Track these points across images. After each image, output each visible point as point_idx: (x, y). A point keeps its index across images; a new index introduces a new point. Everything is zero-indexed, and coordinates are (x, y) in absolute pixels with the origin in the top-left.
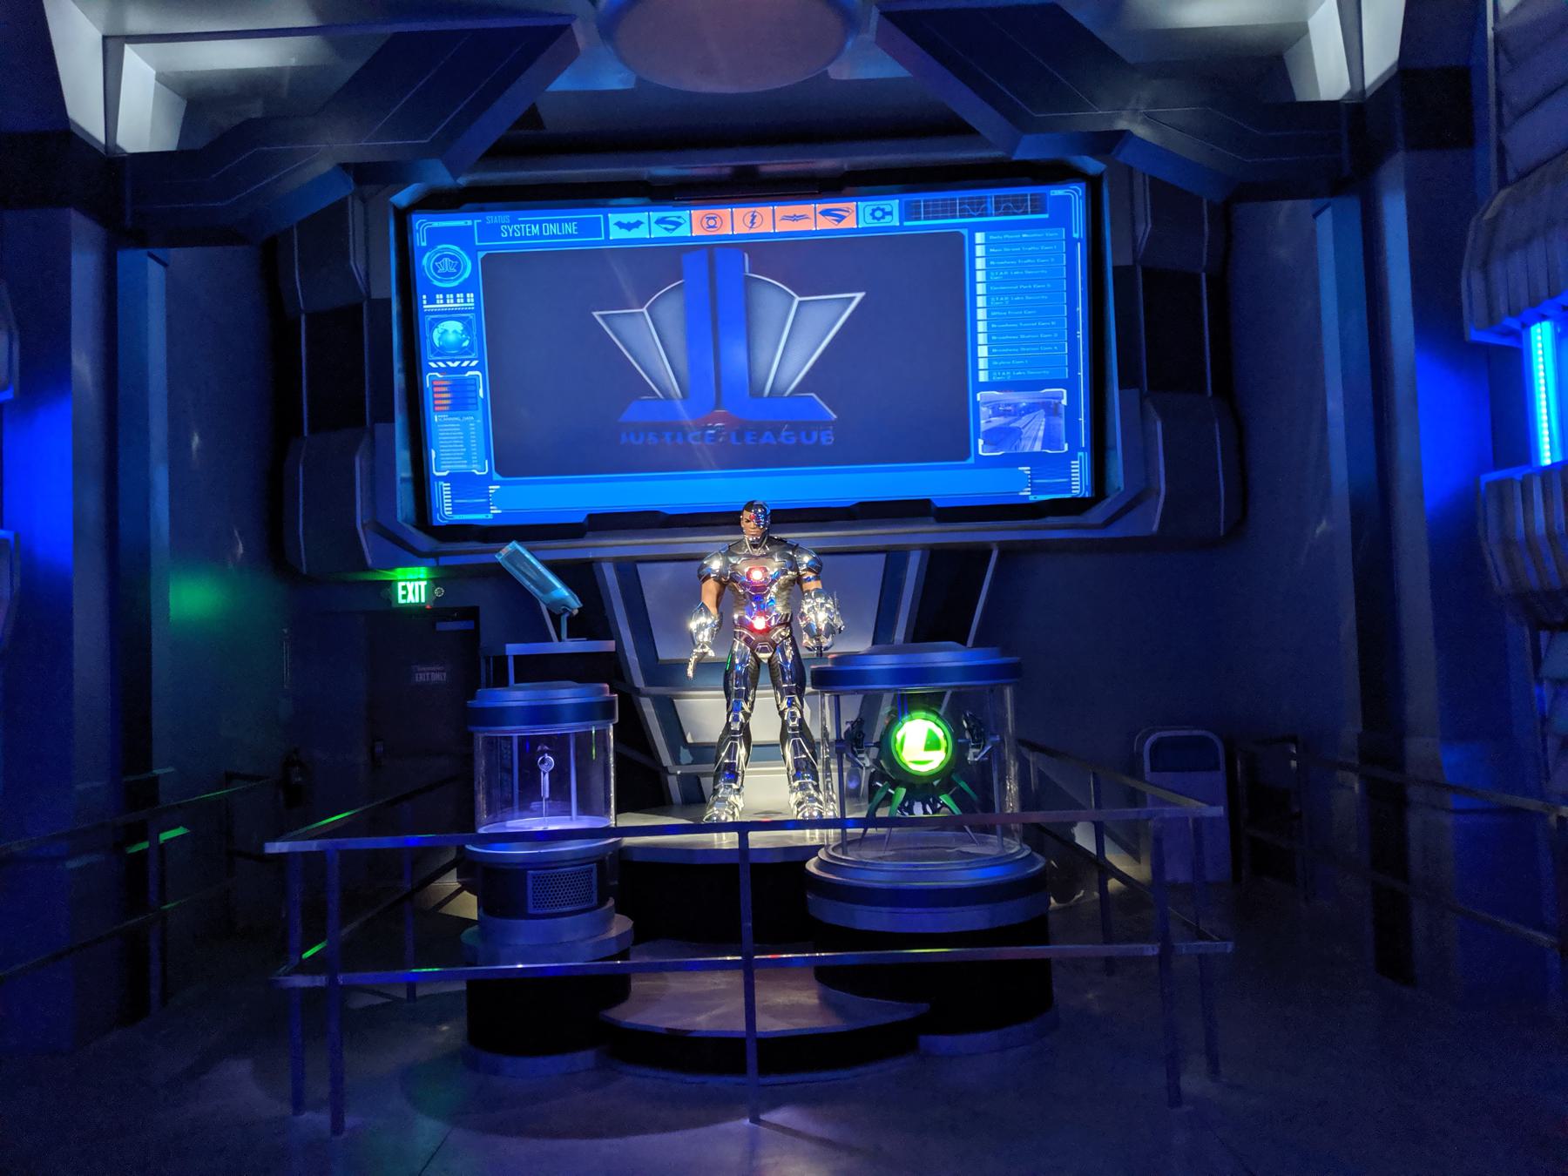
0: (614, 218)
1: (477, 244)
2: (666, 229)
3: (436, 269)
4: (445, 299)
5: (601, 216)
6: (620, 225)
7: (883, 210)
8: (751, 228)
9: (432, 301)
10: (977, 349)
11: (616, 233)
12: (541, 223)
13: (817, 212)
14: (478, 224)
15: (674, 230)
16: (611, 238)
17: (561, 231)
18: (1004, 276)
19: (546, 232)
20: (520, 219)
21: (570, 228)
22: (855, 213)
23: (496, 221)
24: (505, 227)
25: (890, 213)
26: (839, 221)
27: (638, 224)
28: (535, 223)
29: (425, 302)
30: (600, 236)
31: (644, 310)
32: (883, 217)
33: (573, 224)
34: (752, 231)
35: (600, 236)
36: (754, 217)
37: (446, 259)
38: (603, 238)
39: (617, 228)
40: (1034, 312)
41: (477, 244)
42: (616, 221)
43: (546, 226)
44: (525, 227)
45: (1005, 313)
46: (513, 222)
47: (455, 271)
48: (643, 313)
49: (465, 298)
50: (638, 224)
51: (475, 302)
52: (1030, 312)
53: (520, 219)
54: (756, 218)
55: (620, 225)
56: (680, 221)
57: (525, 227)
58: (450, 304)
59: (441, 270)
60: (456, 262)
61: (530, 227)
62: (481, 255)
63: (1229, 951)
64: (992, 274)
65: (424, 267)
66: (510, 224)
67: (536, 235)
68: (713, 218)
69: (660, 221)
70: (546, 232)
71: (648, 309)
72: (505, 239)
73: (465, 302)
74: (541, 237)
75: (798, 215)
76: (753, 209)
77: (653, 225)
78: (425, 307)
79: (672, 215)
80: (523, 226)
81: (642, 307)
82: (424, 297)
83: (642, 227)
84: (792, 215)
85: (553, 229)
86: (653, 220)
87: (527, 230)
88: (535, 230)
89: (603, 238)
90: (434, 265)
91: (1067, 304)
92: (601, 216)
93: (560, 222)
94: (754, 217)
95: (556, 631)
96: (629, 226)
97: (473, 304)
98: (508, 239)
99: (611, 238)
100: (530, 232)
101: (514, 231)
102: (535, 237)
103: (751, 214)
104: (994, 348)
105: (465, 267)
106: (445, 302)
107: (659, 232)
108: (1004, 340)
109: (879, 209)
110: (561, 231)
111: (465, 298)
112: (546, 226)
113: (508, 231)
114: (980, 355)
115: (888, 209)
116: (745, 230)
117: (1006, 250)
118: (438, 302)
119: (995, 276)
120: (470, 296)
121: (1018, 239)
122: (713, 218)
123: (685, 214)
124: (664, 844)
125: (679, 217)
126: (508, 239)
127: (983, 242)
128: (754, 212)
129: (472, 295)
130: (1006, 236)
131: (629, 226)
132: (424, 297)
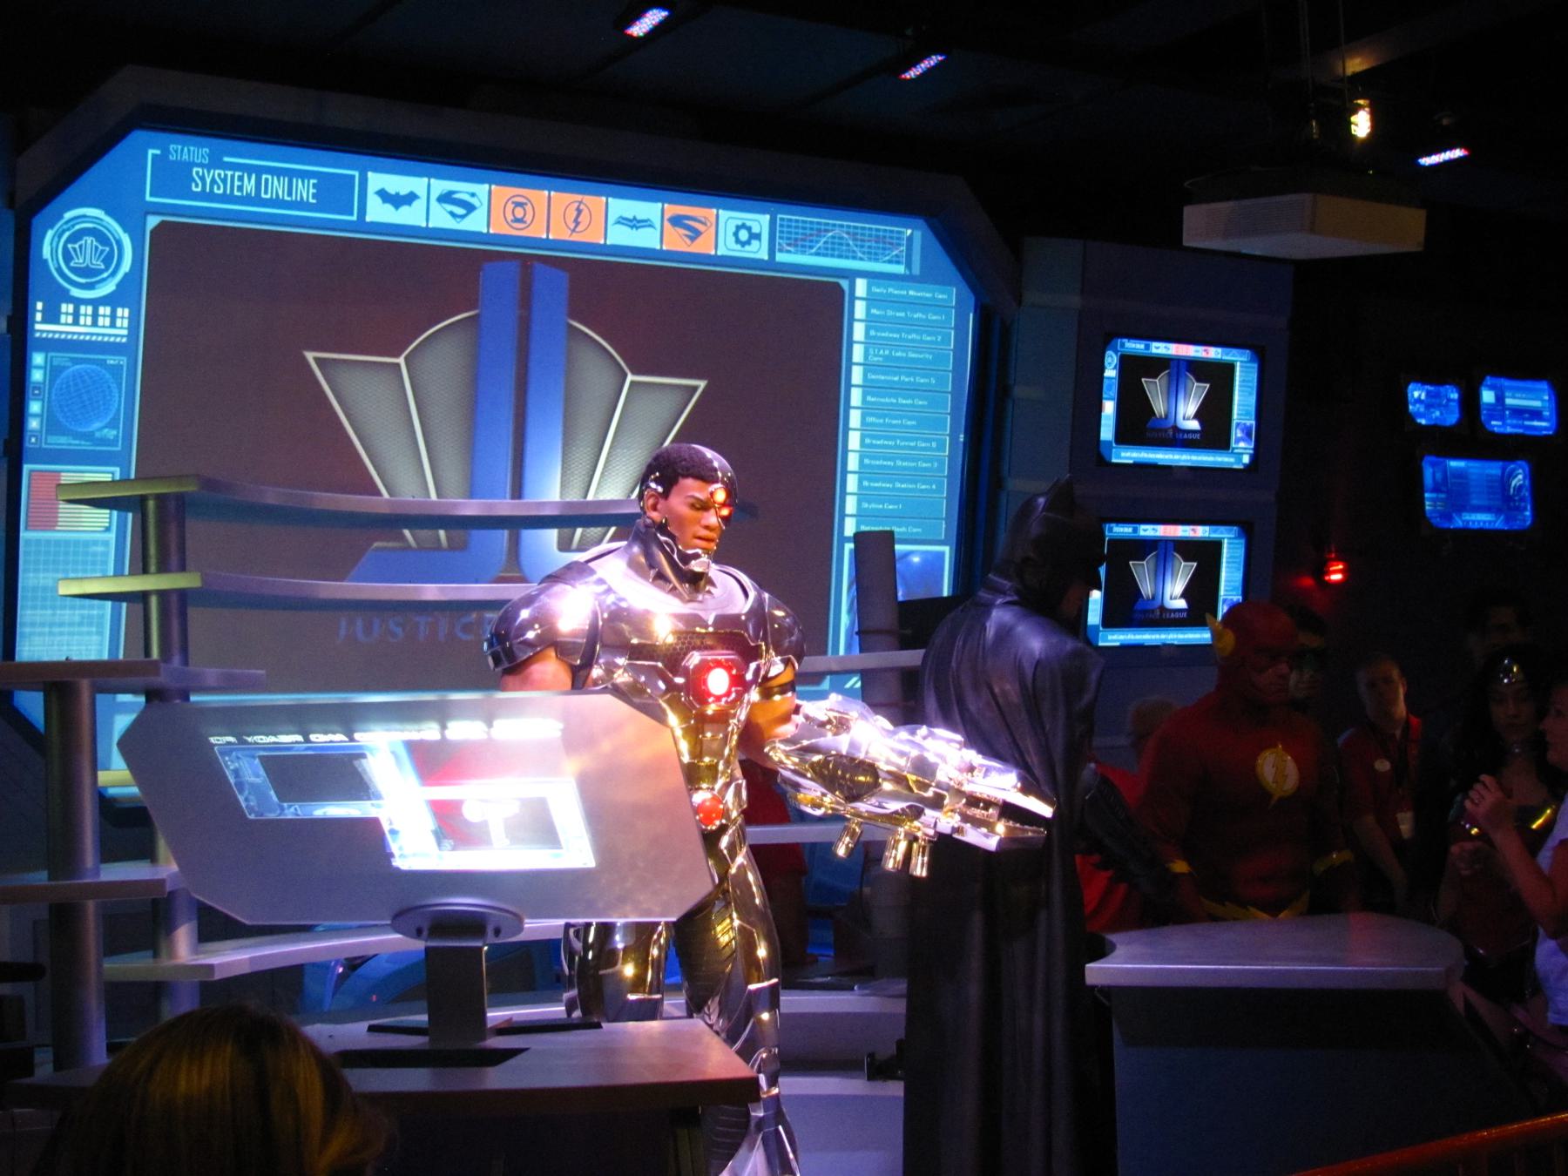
0: (378, 180)
1: (148, 198)
2: (452, 214)
3: (67, 257)
4: (76, 315)
5: (356, 174)
6: (384, 195)
7: (749, 229)
8: (574, 231)
9: (52, 316)
10: (846, 477)
11: (378, 212)
12: (259, 171)
13: (666, 217)
14: (154, 155)
15: (463, 217)
16: (368, 219)
17: (290, 194)
18: (886, 358)
19: (266, 193)
20: (226, 159)
21: (305, 190)
22: (714, 227)
23: (185, 157)
24: (200, 170)
25: (757, 237)
26: (693, 239)
27: (410, 198)
28: (249, 169)
29: (39, 317)
30: (351, 214)
31: (401, 360)
32: (748, 242)
33: (312, 181)
34: (576, 238)
35: (351, 214)
36: (579, 211)
37: (89, 240)
38: (354, 218)
39: (378, 200)
40: (914, 423)
41: (148, 198)
42: (378, 188)
43: (267, 180)
44: (233, 177)
45: (881, 421)
46: (215, 163)
47: (103, 267)
48: (398, 365)
49: (113, 317)
50: (410, 198)
51: (129, 328)
52: (905, 464)
53: (226, 159)
54: (583, 214)
55: (384, 195)
56: (473, 201)
57: (233, 177)
58: (84, 330)
59: (78, 262)
60: (107, 249)
61: (241, 179)
62: (153, 221)
63: (1419, 421)
64: (871, 351)
65: (46, 261)
66: (209, 167)
67: (248, 195)
68: (517, 220)
69: (446, 198)
70: (266, 193)
71: (406, 359)
72: (196, 196)
73: (113, 325)
74: (256, 200)
75: (639, 218)
76: (579, 197)
77: (433, 202)
78: (38, 327)
79: (462, 188)
80: (229, 173)
81: (397, 355)
82: (39, 306)
83: (416, 203)
84: (631, 217)
85: (277, 187)
86: (434, 195)
87: (237, 183)
88: (249, 185)
89: (354, 218)
90: (65, 249)
91: (949, 435)
92: (356, 174)
93: (291, 174)
94: (579, 211)
95: (93, 499)
96: (398, 201)
97: (125, 332)
98: (203, 196)
99: (368, 219)
100: (240, 188)
101: (213, 181)
102: (246, 200)
103: (576, 205)
104: (869, 436)
105: (119, 243)
106: (76, 322)
107: (441, 218)
108: (887, 404)
109: (743, 226)
110: (290, 194)
111: (113, 317)
112: (267, 180)
113: (203, 179)
114: (850, 448)
115: (755, 230)
116: (565, 235)
117: (890, 313)
118: (63, 318)
119: (875, 355)
120: (124, 312)
121: (903, 296)
122: (517, 220)
123: (482, 189)
124: (202, 702)
125: (473, 195)
126: (203, 196)
127: (864, 296)
128: (581, 202)
129: (126, 312)
130: (890, 290)
131: (398, 201)
132: (39, 306)
